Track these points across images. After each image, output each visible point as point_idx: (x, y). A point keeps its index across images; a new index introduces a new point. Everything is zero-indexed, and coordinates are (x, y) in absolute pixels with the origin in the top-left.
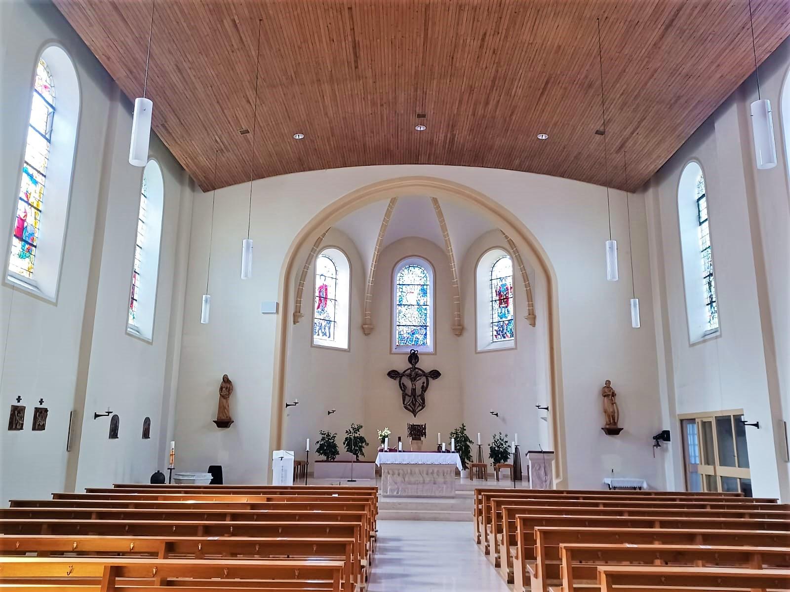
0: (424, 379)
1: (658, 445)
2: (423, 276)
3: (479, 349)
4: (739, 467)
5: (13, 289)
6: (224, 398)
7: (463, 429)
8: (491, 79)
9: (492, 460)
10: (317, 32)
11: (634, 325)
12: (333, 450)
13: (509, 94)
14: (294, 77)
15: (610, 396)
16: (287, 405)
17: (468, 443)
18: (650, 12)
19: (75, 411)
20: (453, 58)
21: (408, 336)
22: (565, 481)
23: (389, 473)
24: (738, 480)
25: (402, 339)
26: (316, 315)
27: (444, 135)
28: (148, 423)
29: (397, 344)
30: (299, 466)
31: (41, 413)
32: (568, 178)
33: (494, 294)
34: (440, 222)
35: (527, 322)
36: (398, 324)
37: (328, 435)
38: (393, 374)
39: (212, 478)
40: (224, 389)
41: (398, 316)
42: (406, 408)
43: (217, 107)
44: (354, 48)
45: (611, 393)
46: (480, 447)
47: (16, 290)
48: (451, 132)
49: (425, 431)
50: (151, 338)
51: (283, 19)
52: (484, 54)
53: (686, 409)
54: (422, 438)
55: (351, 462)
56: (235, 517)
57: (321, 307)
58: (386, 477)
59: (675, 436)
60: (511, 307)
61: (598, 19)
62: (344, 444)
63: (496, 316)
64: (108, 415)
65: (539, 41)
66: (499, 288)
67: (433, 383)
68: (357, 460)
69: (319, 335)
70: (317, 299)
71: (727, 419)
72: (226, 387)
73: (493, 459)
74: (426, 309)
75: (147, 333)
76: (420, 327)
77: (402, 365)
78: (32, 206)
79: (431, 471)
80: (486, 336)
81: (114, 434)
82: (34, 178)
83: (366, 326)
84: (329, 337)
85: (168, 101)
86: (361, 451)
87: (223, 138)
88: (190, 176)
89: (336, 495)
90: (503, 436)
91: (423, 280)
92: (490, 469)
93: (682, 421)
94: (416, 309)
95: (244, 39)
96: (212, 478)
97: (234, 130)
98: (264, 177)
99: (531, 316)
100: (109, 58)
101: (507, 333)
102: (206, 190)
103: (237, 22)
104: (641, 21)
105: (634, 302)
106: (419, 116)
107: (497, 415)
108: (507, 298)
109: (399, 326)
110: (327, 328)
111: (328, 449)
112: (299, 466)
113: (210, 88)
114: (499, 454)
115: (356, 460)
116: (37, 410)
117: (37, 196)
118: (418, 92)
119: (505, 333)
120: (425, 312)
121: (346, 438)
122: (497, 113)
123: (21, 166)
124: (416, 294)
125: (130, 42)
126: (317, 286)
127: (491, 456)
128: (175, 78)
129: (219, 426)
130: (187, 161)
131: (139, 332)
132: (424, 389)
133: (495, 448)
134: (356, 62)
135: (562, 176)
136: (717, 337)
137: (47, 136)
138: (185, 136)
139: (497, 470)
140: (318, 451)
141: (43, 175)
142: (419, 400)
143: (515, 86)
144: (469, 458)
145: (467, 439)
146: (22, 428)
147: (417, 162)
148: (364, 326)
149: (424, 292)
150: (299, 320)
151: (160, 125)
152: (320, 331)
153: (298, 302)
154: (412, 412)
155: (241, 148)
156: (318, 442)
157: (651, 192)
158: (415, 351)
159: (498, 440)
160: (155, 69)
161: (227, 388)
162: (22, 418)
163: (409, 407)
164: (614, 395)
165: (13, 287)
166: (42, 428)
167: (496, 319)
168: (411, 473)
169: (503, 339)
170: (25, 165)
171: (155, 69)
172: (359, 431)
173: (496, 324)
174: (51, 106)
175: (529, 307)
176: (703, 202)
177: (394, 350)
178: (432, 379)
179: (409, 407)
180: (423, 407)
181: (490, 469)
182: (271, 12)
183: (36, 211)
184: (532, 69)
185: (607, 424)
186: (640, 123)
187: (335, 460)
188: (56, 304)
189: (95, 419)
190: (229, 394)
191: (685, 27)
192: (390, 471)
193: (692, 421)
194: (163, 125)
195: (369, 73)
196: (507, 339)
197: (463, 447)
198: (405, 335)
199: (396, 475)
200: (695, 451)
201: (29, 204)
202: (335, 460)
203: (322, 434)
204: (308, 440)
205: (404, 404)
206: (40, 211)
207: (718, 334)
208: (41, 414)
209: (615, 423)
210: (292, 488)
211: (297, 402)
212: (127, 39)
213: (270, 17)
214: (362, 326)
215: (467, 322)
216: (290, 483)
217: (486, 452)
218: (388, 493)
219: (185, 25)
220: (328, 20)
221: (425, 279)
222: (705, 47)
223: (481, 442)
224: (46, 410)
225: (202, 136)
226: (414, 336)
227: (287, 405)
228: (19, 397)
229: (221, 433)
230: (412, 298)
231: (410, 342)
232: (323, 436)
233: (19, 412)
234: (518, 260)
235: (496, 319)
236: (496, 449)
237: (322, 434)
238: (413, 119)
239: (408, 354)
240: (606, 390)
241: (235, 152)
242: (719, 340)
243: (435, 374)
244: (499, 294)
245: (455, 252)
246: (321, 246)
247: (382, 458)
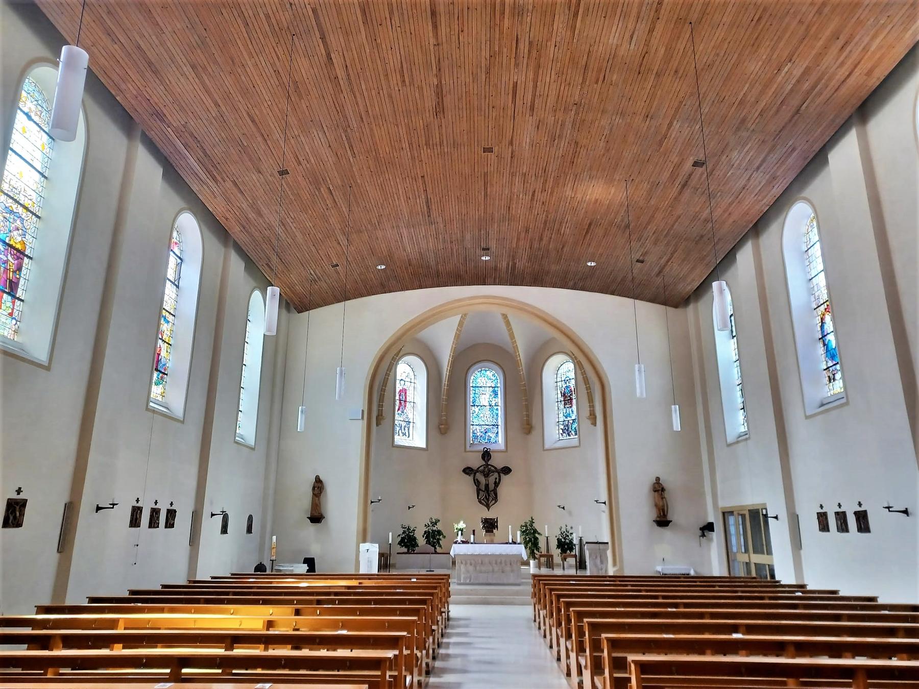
0: (496, 475)
1: (703, 535)
2: (494, 379)
3: (546, 447)
4: (767, 554)
6: (317, 497)
7: (532, 522)
8: (543, 221)
9: (559, 551)
10: (396, 194)
11: (675, 429)
12: (413, 543)
13: (559, 233)
14: (377, 224)
15: (660, 492)
16: (372, 502)
17: (537, 535)
18: (668, 175)
19: (195, 511)
20: (509, 208)
21: (481, 434)
22: (622, 568)
23: (462, 563)
24: (767, 566)
25: (476, 437)
26: (397, 417)
27: (506, 263)
28: (251, 520)
29: (471, 442)
30: (383, 558)
31: (172, 513)
32: (617, 295)
33: (560, 395)
34: (508, 330)
35: (589, 422)
36: (472, 423)
37: (409, 529)
38: (468, 471)
39: (308, 568)
40: (316, 489)
41: (471, 416)
42: (480, 502)
43: (313, 248)
44: (427, 202)
45: (660, 489)
46: (547, 539)
47: (156, 414)
48: (512, 260)
49: (497, 524)
50: (253, 444)
51: (369, 186)
52: (535, 205)
53: (726, 503)
54: (494, 530)
55: (429, 553)
56: (336, 594)
57: (401, 409)
58: (460, 567)
59: (719, 527)
60: (574, 407)
62: (423, 537)
63: (561, 415)
64: (113, 508)
65: (579, 196)
66: (563, 390)
67: (505, 478)
68: (436, 551)
69: (399, 435)
70: (398, 401)
71: (757, 512)
72: (318, 487)
73: (560, 550)
74: (497, 409)
75: (251, 441)
76: (492, 427)
77: (476, 462)
78: (165, 342)
79: (500, 561)
80: (552, 433)
81: (224, 530)
82: (167, 318)
83: (443, 426)
84: (409, 437)
85: (273, 246)
86: (439, 543)
87: (317, 271)
88: (286, 300)
89: (415, 580)
90: (569, 528)
91: (494, 383)
92: (557, 559)
93: (724, 513)
94: (488, 409)
95: (337, 200)
96: (308, 568)
97: (326, 265)
98: (351, 299)
99: (592, 416)
100: (227, 219)
101: (572, 431)
102: (299, 312)
103: (331, 188)
104: (661, 182)
105: (675, 409)
106: (484, 249)
107: (563, 508)
108: (571, 399)
109: (473, 425)
110: (406, 429)
111: (408, 541)
112: (383, 558)
113: (308, 236)
114: (565, 546)
115: (434, 552)
117: (169, 333)
118: (482, 232)
119: (570, 431)
120: (497, 412)
121: (425, 532)
122: (551, 247)
123: (160, 313)
124: (488, 396)
125: (245, 206)
126: (398, 390)
127: (558, 547)
128: (279, 230)
129: (312, 522)
130: (285, 290)
131: (243, 439)
132: (497, 484)
133: (561, 539)
134: (429, 212)
135: (612, 293)
136: (746, 439)
137: (176, 283)
138: (285, 271)
139: (564, 559)
140: (400, 543)
141: (173, 315)
142: (492, 494)
143: (564, 227)
144: (538, 549)
145: (535, 531)
146: (158, 527)
147: (484, 283)
148: (440, 426)
149: (496, 394)
150: (382, 422)
151: (264, 265)
152: (400, 431)
153: (380, 406)
154: (485, 506)
155: (331, 278)
156: (399, 535)
157: (691, 307)
158: (488, 449)
159: (564, 532)
160: (264, 225)
161: (318, 488)
162: (158, 518)
163: (483, 501)
164: (663, 490)
165: (154, 411)
166: (172, 526)
167: (562, 418)
168: (482, 563)
169: (568, 437)
170: (164, 311)
171: (264, 225)
172: (436, 525)
173: (562, 423)
174: (180, 258)
175: (590, 408)
176: (733, 318)
177: (468, 448)
178: (503, 475)
179: (483, 501)
180: (496, 502)
181: (557, 559)
182: (359, 181)
183: (167, 345)
184: (576, 215)
185: (658, 517)
186: (672, 254)
187: (415, 552)
188: (183, 422)
190: (321, 493)
191: (698, 186)
192: (463, 561)
193: (731, 513)
194: (267, 264)
195: (440, 220)
196: (572, 437)
197: (531, 538)
198: (478, 434)
199: (468, 565)
200: (736, 542)
201: (163, 341)
202: (415, 552)
203: (403, 528)
204: (390, 534)
205: (478, 498)
206: (171, 345)
207: (747, 436)
208: (171, 514)
209: (665, 515)
210: (378, 575)
211: (380, 499)
212: (242, 205)
213: (359, 185)
214: (439, 426)
215: (535, 421)
216: (377, 573)
217: (554, 543)
218: (462, 581)
219: (289, 193)
220: (405, 184)
221: (496, 381)
222: (716, 201)
223: (548, 534)
225: (299, 271)
226: (487, 434)
227: (372, 502)
229: (312, 528)
230: (484, 400)
231: (483, 440)
232: (404, 529)
233: (156, 514)
234: (578, 365)
235: (562, 418)
236: (563, 540)
237: (403, 528)
238: (478, 251)
239: (480, 451)
240: (656, 486)
241: (327, 281)
242: (748, 441)
243: (507, 470)
244: (564, 395)
245: (522, 355)
246: (400, 355)
247: (457, 550)
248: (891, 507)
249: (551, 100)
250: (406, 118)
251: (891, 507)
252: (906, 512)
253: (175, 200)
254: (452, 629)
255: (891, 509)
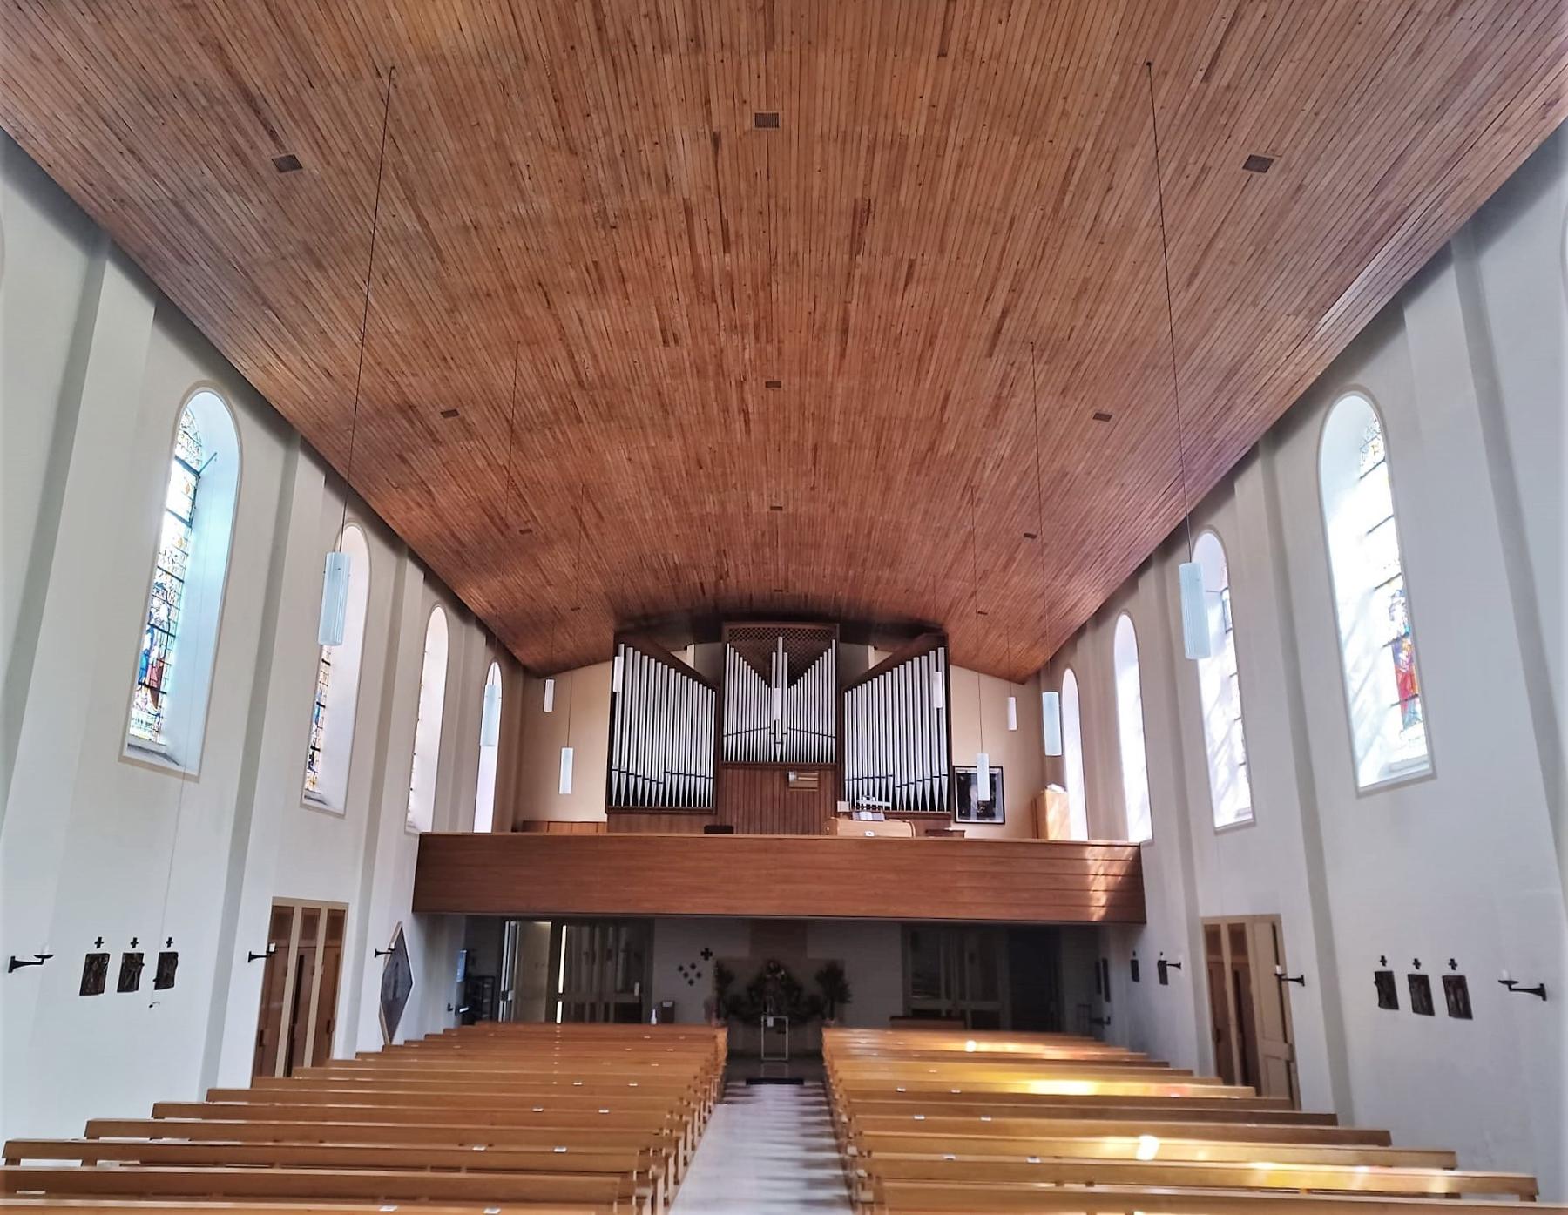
5: (184, 778)
61: (1149, 64)
116: (128, 957)
170: (159, 572)
189: (11, 971)
208: (168, 963)
224: (175, 955)
228: (170, 939)
248: (1516, 982)
249: (658, 229)
250: (930, 209)
251: (1516, 982)
252: (1540, 991)
253: (180, 365)
254: (837, 1176)
255: (1513, 986)
